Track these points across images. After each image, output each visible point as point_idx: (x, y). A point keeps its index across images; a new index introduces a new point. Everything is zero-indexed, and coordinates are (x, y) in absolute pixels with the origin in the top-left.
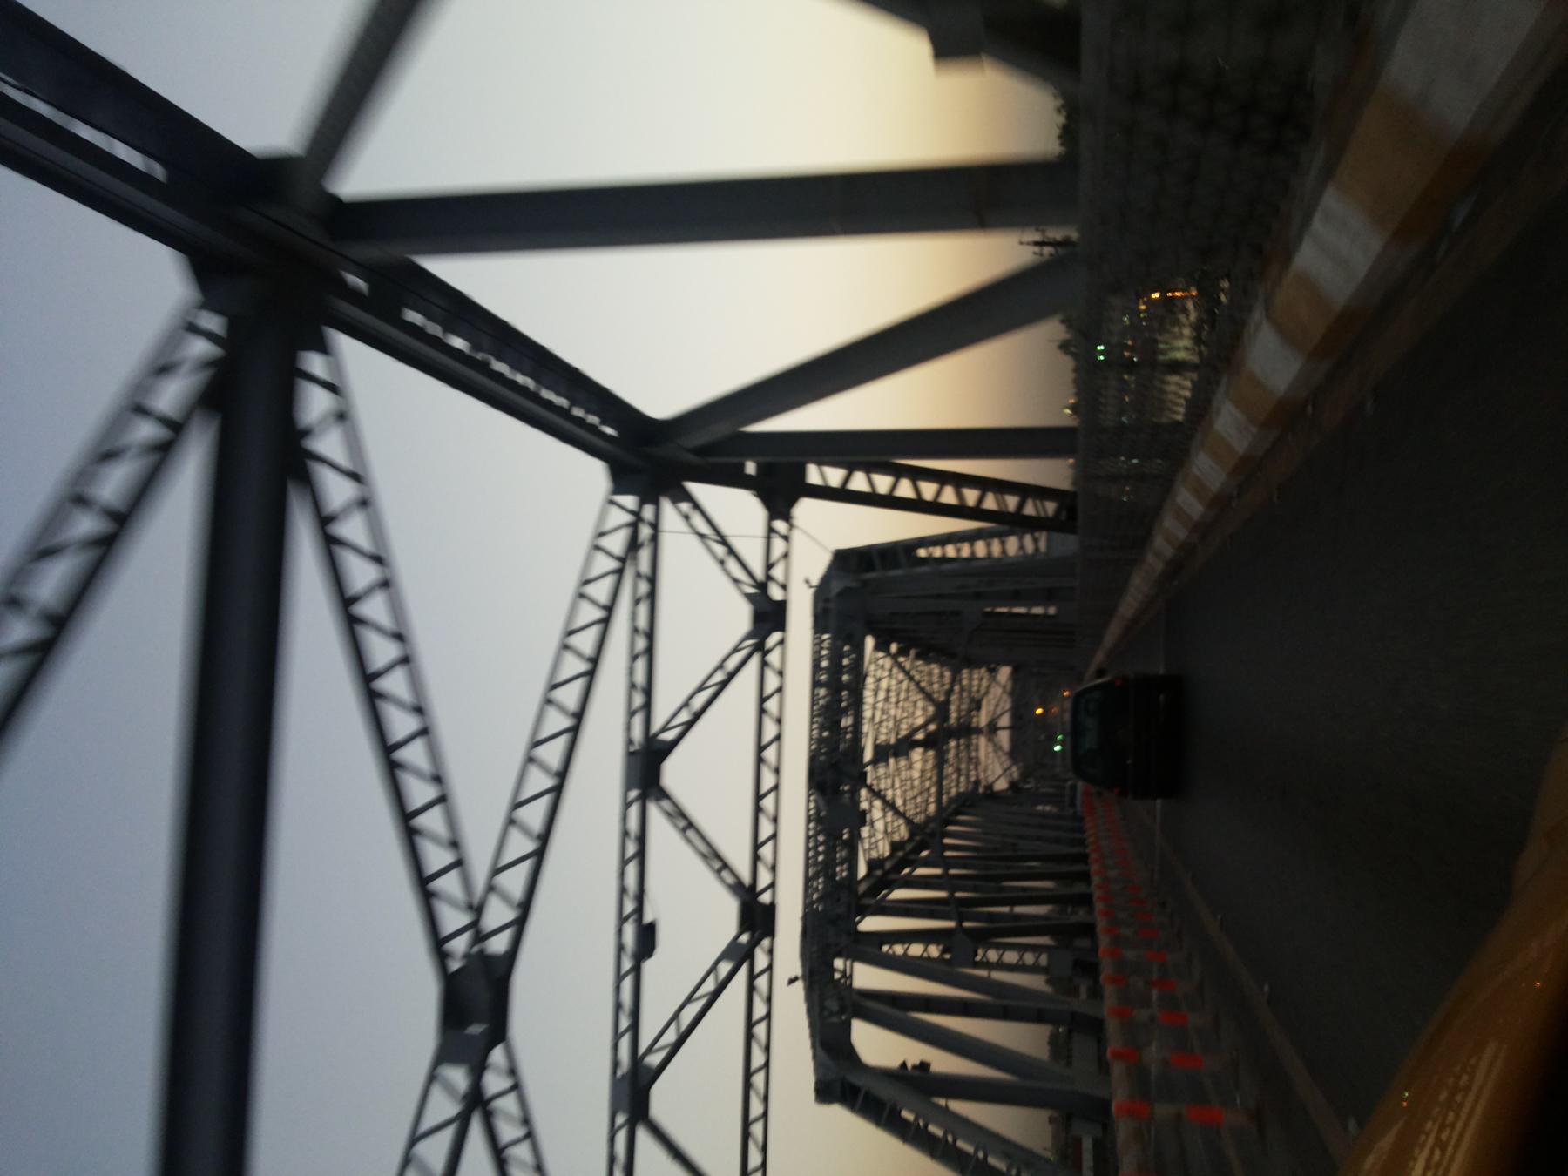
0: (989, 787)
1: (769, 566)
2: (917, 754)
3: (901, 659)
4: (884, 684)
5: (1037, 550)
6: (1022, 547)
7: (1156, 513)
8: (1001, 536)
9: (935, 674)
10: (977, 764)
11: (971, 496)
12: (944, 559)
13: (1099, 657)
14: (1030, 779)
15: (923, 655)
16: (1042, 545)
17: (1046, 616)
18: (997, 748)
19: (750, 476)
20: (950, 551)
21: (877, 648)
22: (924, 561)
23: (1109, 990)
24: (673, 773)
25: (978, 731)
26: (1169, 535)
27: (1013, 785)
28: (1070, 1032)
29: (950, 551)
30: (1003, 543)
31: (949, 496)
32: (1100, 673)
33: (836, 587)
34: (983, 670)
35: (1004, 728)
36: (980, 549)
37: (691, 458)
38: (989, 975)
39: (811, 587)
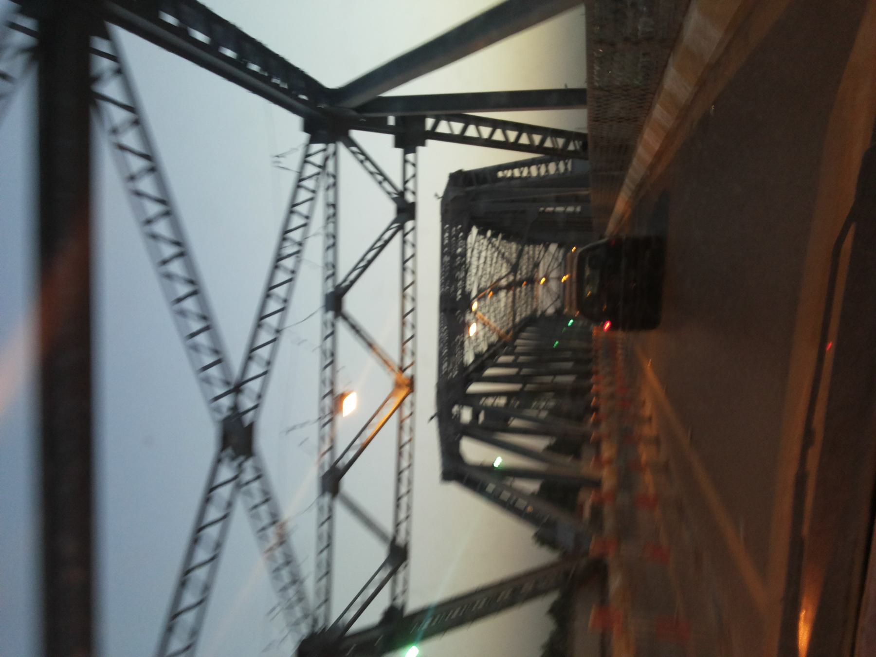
1: (405, 182)
2: (502, 294)
3: (494, 240)
4: (483, 254)
5: (566, 169)
6: (557, 169)
8: (547, 162)
10: (537, 299)
11: (512, 135)
12: (512, 178)
15: (507, 237)
16: (569, 166)
17: (574, 213)
19: (392, 126)
20: (517, 172)
21: (479, 233)
22: (504, 178)
24: (351, 302)
29: (517, 172)
30: (547, 166)
31: (498, 136)
33: (451, 196)
34: (542, 246)
36: (534, 170)
37: (354, 113)
39: (439, 198)
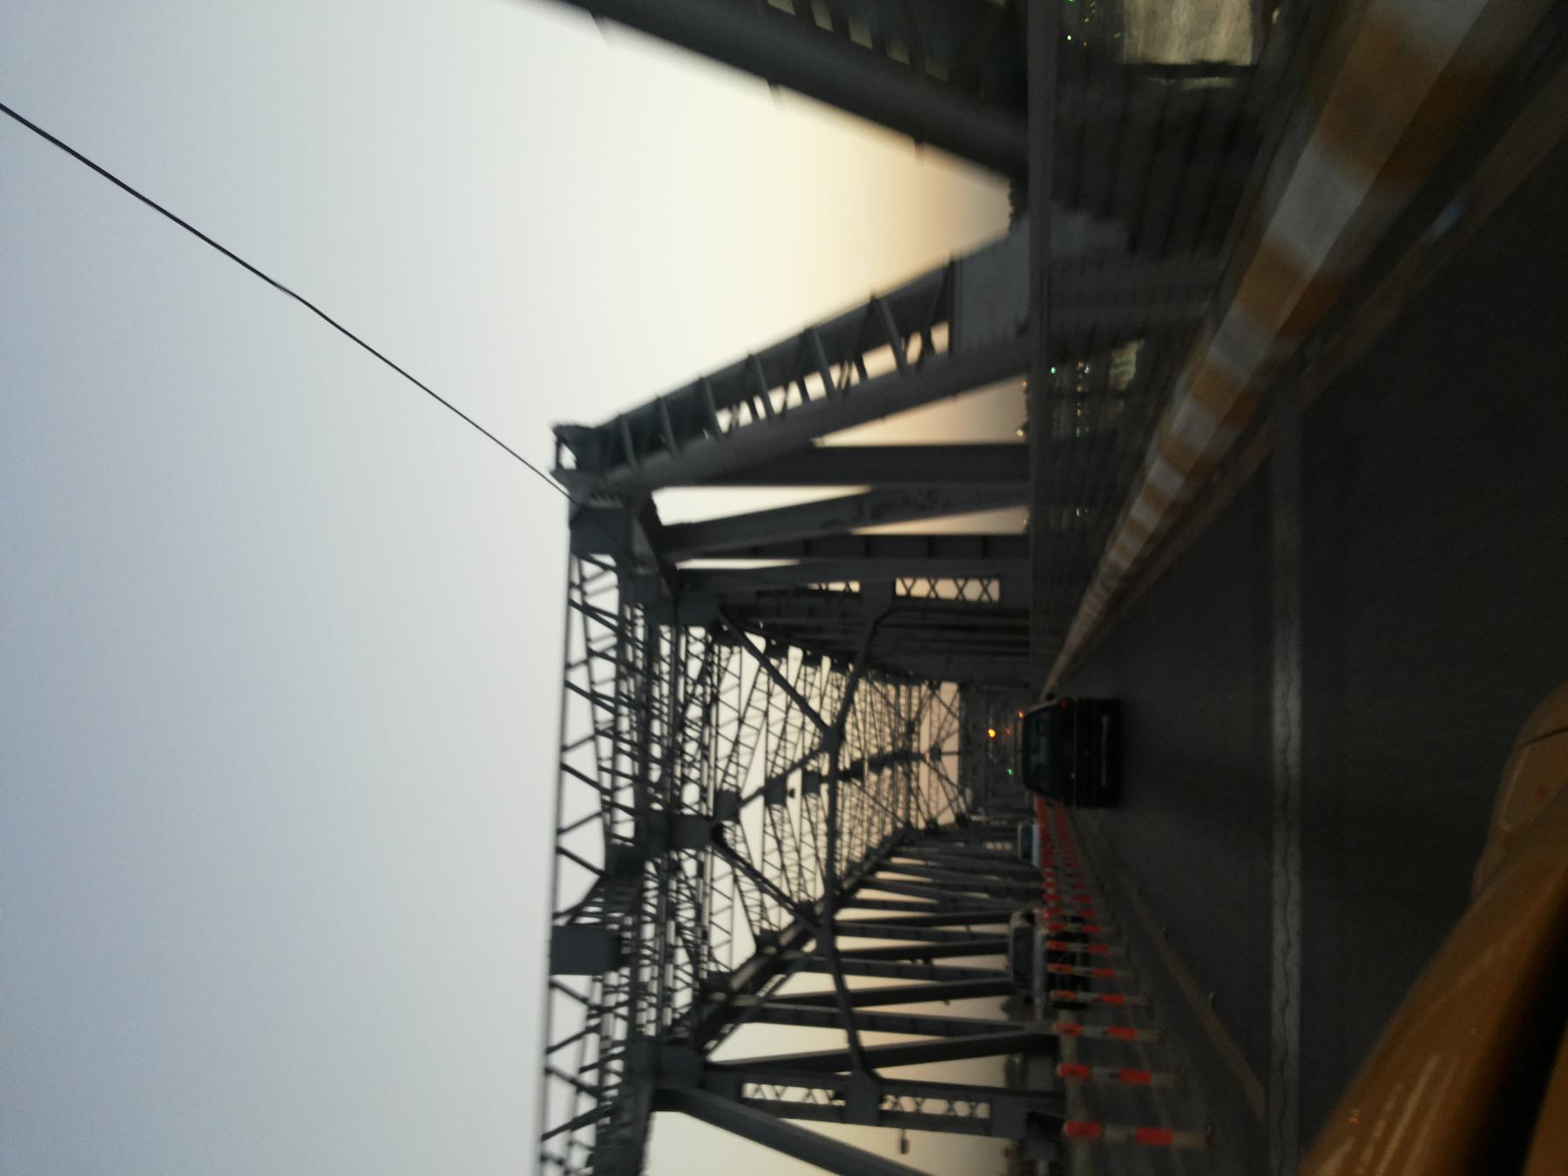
0: (932, 822)
13: (1051, 682)
14: (981, 810)
18: (942, 777)
25: (919, 757)
26: (1121, 553)
27: (960, 818)
28: (1025, 1062)
32: (1050, 697)
35: (950, 753)
38: (968, 929)
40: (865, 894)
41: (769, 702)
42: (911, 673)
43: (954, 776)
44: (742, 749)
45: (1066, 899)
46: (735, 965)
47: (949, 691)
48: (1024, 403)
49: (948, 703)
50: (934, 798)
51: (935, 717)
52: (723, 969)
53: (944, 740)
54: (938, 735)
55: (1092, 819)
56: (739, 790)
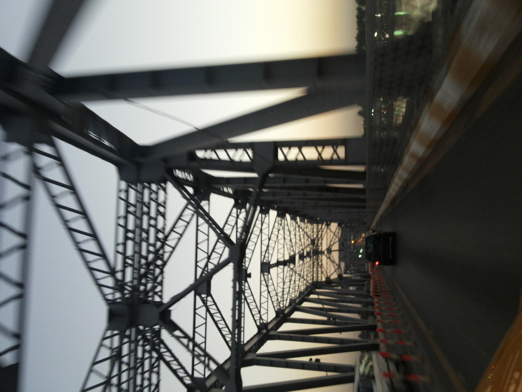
0: (328, 278)
7: (392, 176)
9: (309, 228)
13: (374, 224)
18: (333, 262)
23: (381, 334)
25: (322, 253)
27: (340, 276)
40: (297, 315)
41: (278, 233)
42: (318, 219)
43: (337, 260)
44: (270, 248)
45: (383, 308)
46: (269, 321)
47: (334, 226)
48: (363, 130)
49: (334, 231)
50: (329, 268)
51: (328, 236)
52: (264, 322)
53: (332, 245)
54: (330, 244)
55: (388, 269)
56: (269, 262)
